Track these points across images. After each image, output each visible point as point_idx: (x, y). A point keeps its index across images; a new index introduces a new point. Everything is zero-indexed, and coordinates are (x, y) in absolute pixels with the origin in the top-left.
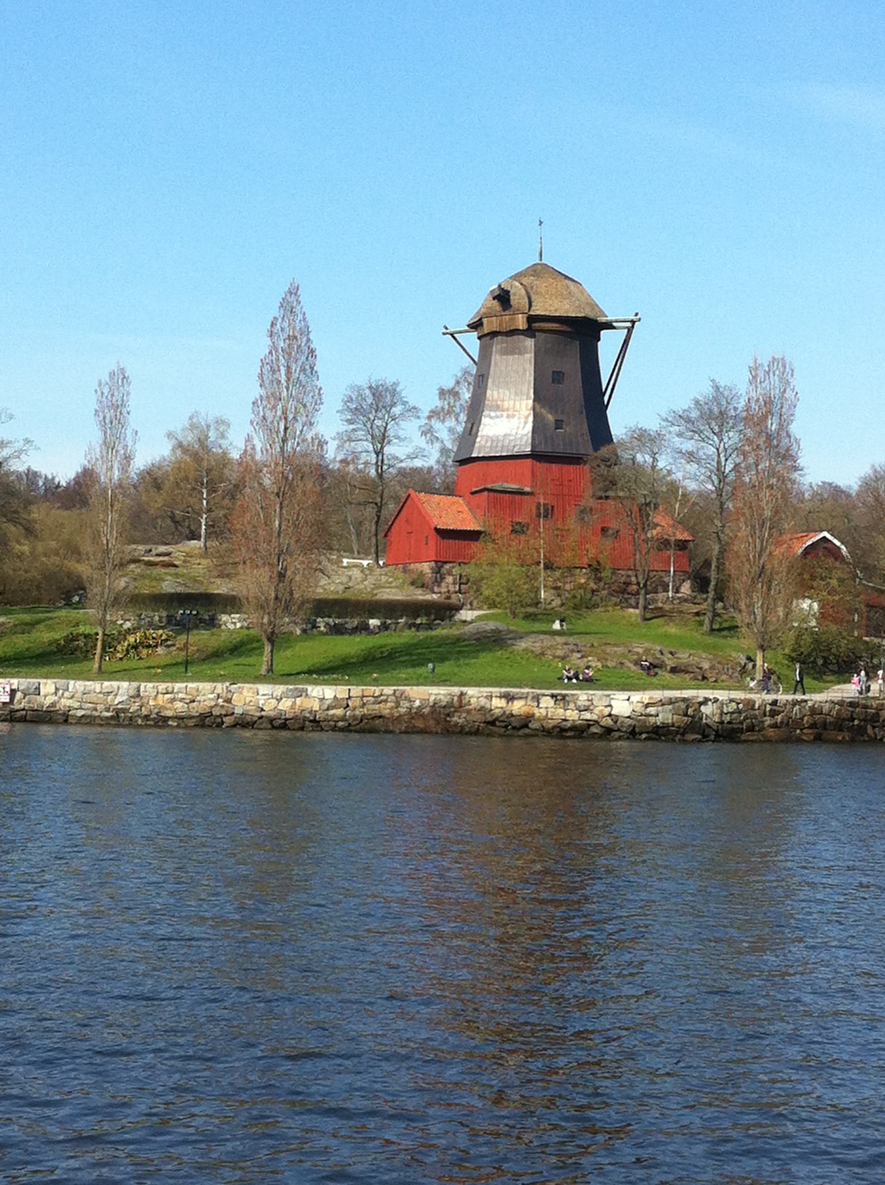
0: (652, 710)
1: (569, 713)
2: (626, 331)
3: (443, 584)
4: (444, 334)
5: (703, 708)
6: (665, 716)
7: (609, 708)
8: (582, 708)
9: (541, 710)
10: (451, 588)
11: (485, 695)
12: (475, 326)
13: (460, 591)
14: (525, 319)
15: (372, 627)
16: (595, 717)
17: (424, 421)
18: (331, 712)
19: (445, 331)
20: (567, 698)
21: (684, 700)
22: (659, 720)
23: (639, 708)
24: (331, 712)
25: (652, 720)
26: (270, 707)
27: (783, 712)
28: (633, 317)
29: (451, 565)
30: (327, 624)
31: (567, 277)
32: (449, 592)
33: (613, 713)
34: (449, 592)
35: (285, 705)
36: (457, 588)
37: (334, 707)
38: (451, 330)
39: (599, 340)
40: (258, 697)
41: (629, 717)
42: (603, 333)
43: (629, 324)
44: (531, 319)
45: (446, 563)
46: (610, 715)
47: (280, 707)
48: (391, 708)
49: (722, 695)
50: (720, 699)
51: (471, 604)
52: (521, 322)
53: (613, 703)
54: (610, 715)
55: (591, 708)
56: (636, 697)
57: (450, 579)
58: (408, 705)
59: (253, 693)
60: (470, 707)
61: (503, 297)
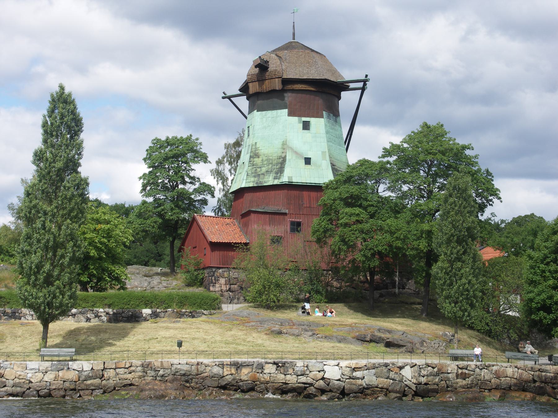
0: (358, 374)
1: (288, 377)
2: (361, 91)
3: (217, 285)
4: (223, 98)
5: (403, 372)
6: (369, 378)
7: (322, 373)
8: (299, 373)
9: (265, 376)
10: (224, 288)
11: (217, 363)
12: (244, 90)
13: (230, 290)
14: (280, 82)
15: (144, 315)
16: (309, 380)
17: (214, 166)
18: (89, 382)
19: (224, 95)
20: (287, 365)
21: (386, 365)
22: (363, 383)
23: (347, 372)
24: (89, 382)
25: (359, 382)
26: (36, 378)
27: (472, 375)
28: (363, 78)
29: (223, 270)
30: (107, 313)
31: (313, 51)
32: (221, 290)
33: (325, 376)
34: (221, 290)
35: (49, 377)
36: (228, 286)
37: (90, 378)
38: (228, 94)
39: (520, 216)
40: (27, 371)
41: (339, 380)
42: (343, 94)
43: (361, 85)
44: (286, 82)
45: (219, 268)
46: (323, 378)
47: (46, 379)
48: (140, 377)
49: (419, 361)
50: (418, 364)
51: (238, 299)
52: (277, 85)
53: (326, 368)
54: (323, 378)
55: (308, 372)
56: (344, 363)
57: (222, 281)
58: (153, 373)
59: (22, 368)
60: (206, 374)
61: (262, 66)
